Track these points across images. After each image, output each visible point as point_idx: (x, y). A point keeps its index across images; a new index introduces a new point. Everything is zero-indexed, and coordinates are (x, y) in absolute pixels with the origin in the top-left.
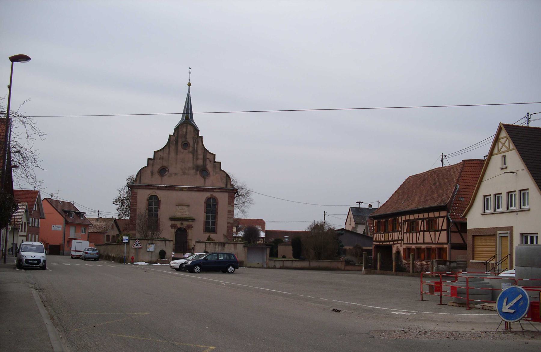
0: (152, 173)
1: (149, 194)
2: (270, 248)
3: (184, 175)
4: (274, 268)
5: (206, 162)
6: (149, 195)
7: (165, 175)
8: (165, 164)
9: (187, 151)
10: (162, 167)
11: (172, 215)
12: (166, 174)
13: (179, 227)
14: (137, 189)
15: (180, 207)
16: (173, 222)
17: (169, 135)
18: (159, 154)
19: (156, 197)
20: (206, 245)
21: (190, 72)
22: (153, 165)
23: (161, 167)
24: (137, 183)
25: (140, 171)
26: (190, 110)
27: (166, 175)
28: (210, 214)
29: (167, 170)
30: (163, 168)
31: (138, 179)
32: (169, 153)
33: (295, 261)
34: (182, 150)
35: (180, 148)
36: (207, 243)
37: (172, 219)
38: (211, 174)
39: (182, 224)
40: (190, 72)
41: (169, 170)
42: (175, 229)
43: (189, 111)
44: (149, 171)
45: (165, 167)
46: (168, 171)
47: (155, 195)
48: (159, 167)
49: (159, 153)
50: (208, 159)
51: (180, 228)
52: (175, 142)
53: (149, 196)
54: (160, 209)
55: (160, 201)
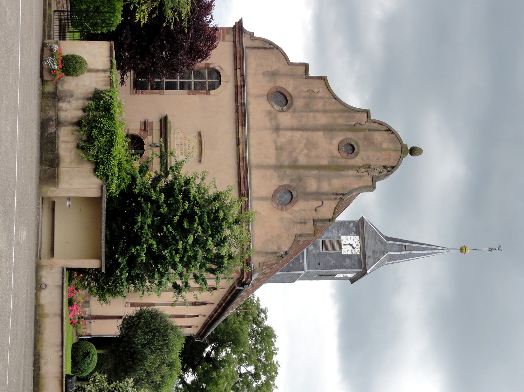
0: (274, 74)
1: (222, 69)
2: (98, 270)
3: (276, 149)
4: (39, 286)
5: (313, 199)
6: (219, 66)
7: (273, 103)
8: (299, 103)
9: (336, 153)
10: (291, 97)
11: (174, 123)
12: (275, 106)
13: (145, 141)
14: (232, 40)
15: (196, 141)
16: (156, 127)
17: (369, 110)
18: (321, 90)
19: (213, 87)
20: (104, 71)
21: (492, 249)
22: (292, 75)
23: (290, 94)
24: (247, 42)
25: (278, 48)
26: (408, 252)
27: (272, 107)
28: (195, 78)
29: (285, 107)
30: (288, 98)
31: (256, 44)
32: (325, 111)
33: (60, 354)
34: (336, 142)
35: (340, 137)
36: (108, 74)
37: (164, 122)
38: (286, 214)
39: (153, 146)
40: (492, 249)
41: (284, 113)
42: (139, 131)
43: (406, 250)
44: (277, 65)
45: (292, 102)
46: (282, 111)
47: (220, 82)
48: (290, 90)
49: (322, 92)
50: (320, 203)
51: (144, 144)
52: (353, 123)
53: (217, 68)
54: (189, 94)
55: (208, 93)
